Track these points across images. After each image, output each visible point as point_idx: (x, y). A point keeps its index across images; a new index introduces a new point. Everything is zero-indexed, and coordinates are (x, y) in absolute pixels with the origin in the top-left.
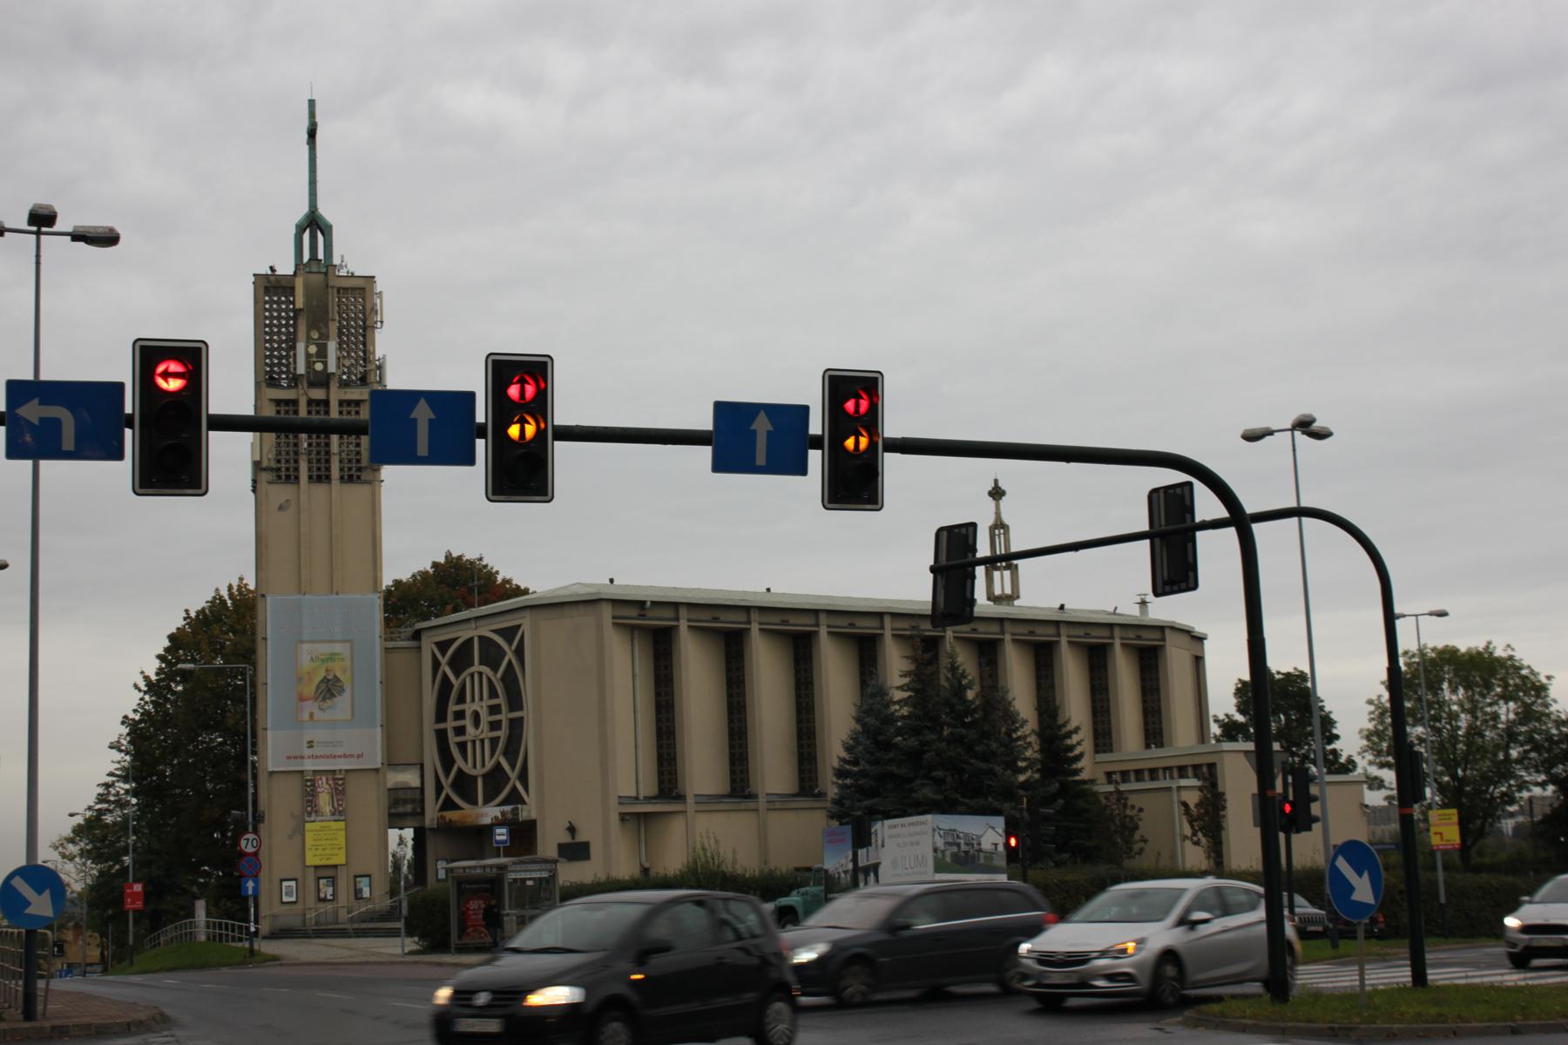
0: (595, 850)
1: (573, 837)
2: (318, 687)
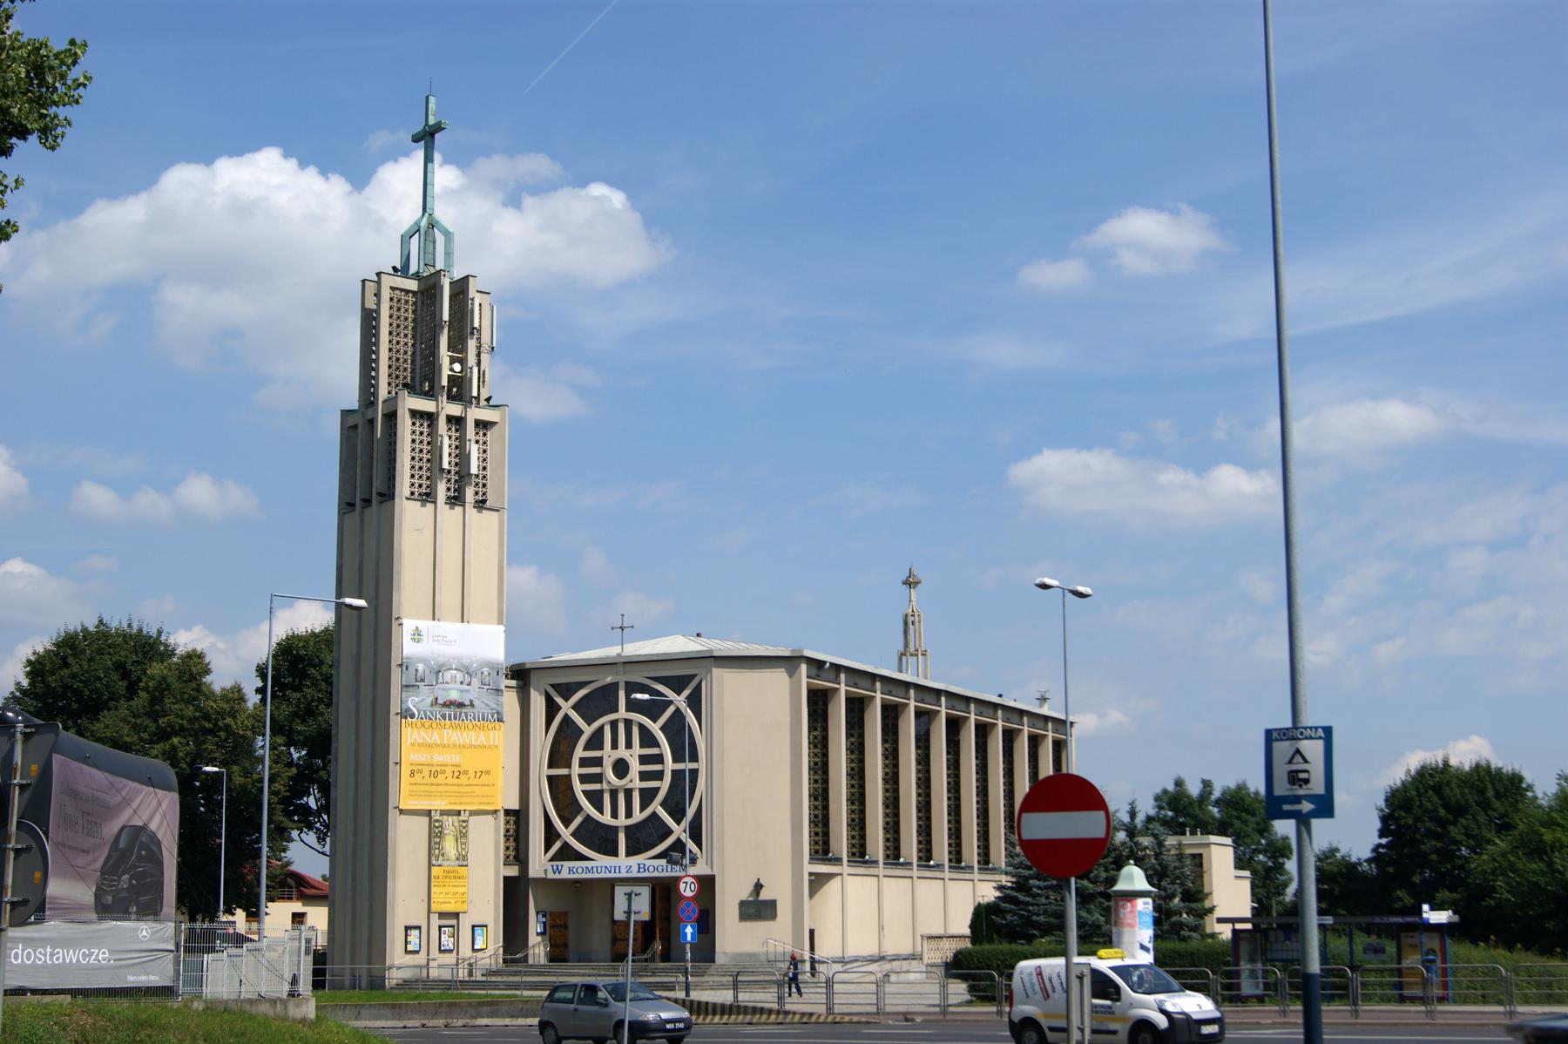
0: (784, 909)
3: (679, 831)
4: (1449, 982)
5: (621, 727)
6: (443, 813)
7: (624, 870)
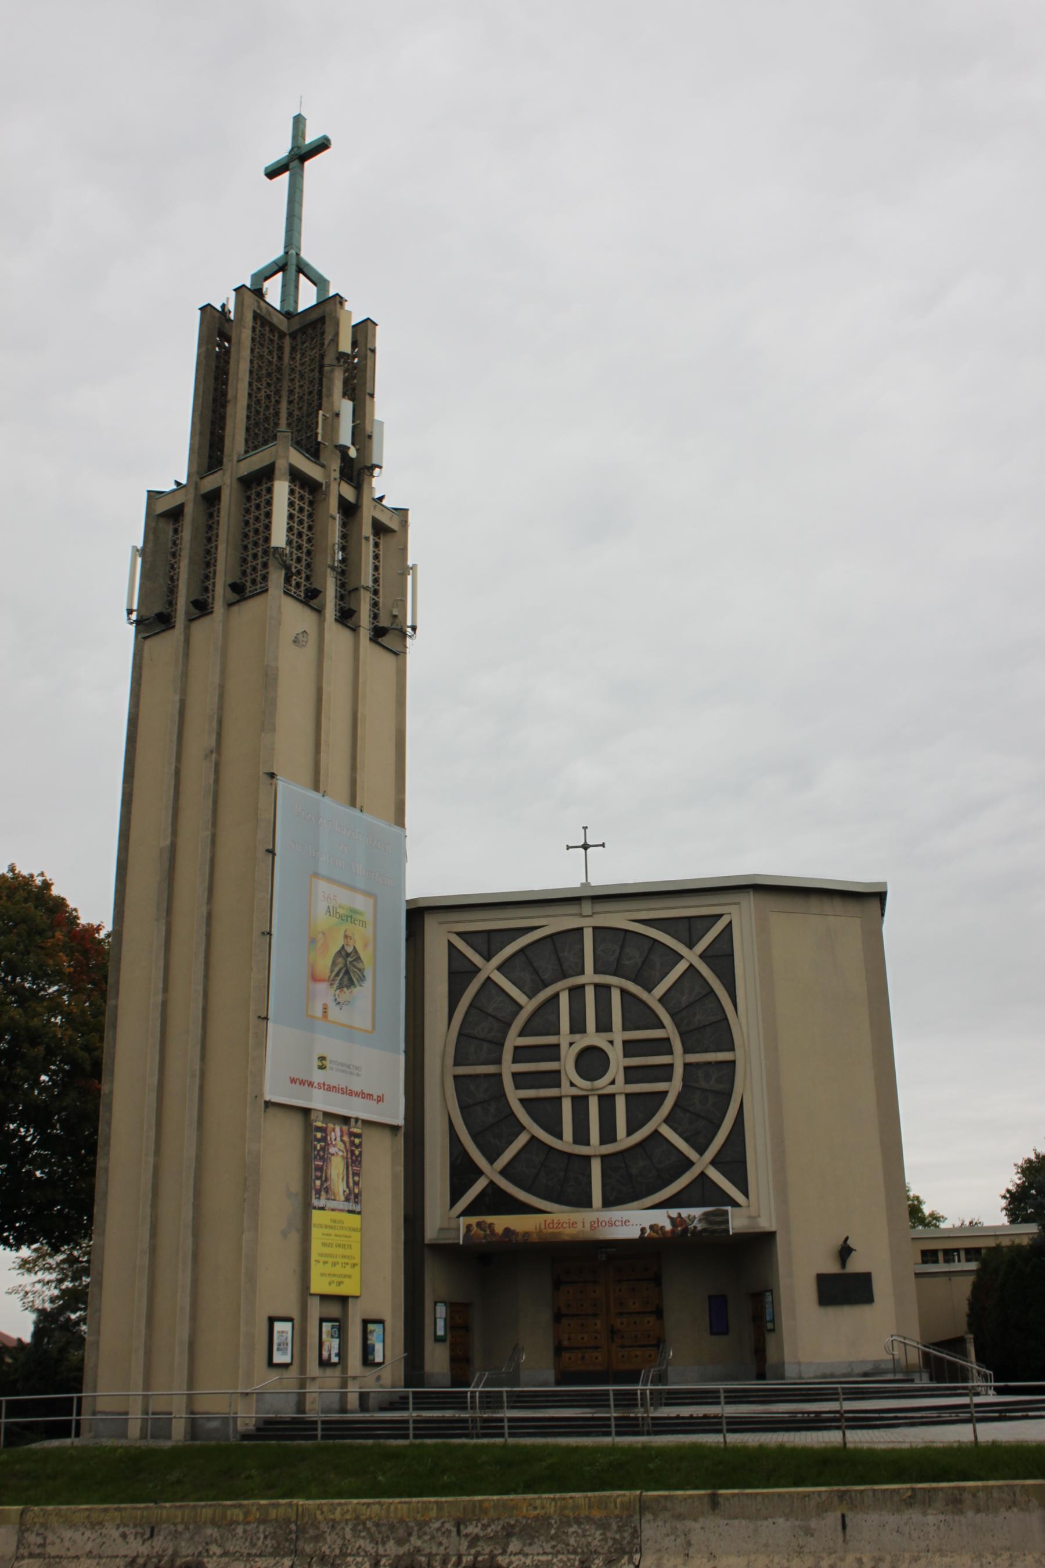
1: (843, 1265)
2: (334, 964)
5: (590, 994)
6: (328, 1116)
7: (580, 1226)
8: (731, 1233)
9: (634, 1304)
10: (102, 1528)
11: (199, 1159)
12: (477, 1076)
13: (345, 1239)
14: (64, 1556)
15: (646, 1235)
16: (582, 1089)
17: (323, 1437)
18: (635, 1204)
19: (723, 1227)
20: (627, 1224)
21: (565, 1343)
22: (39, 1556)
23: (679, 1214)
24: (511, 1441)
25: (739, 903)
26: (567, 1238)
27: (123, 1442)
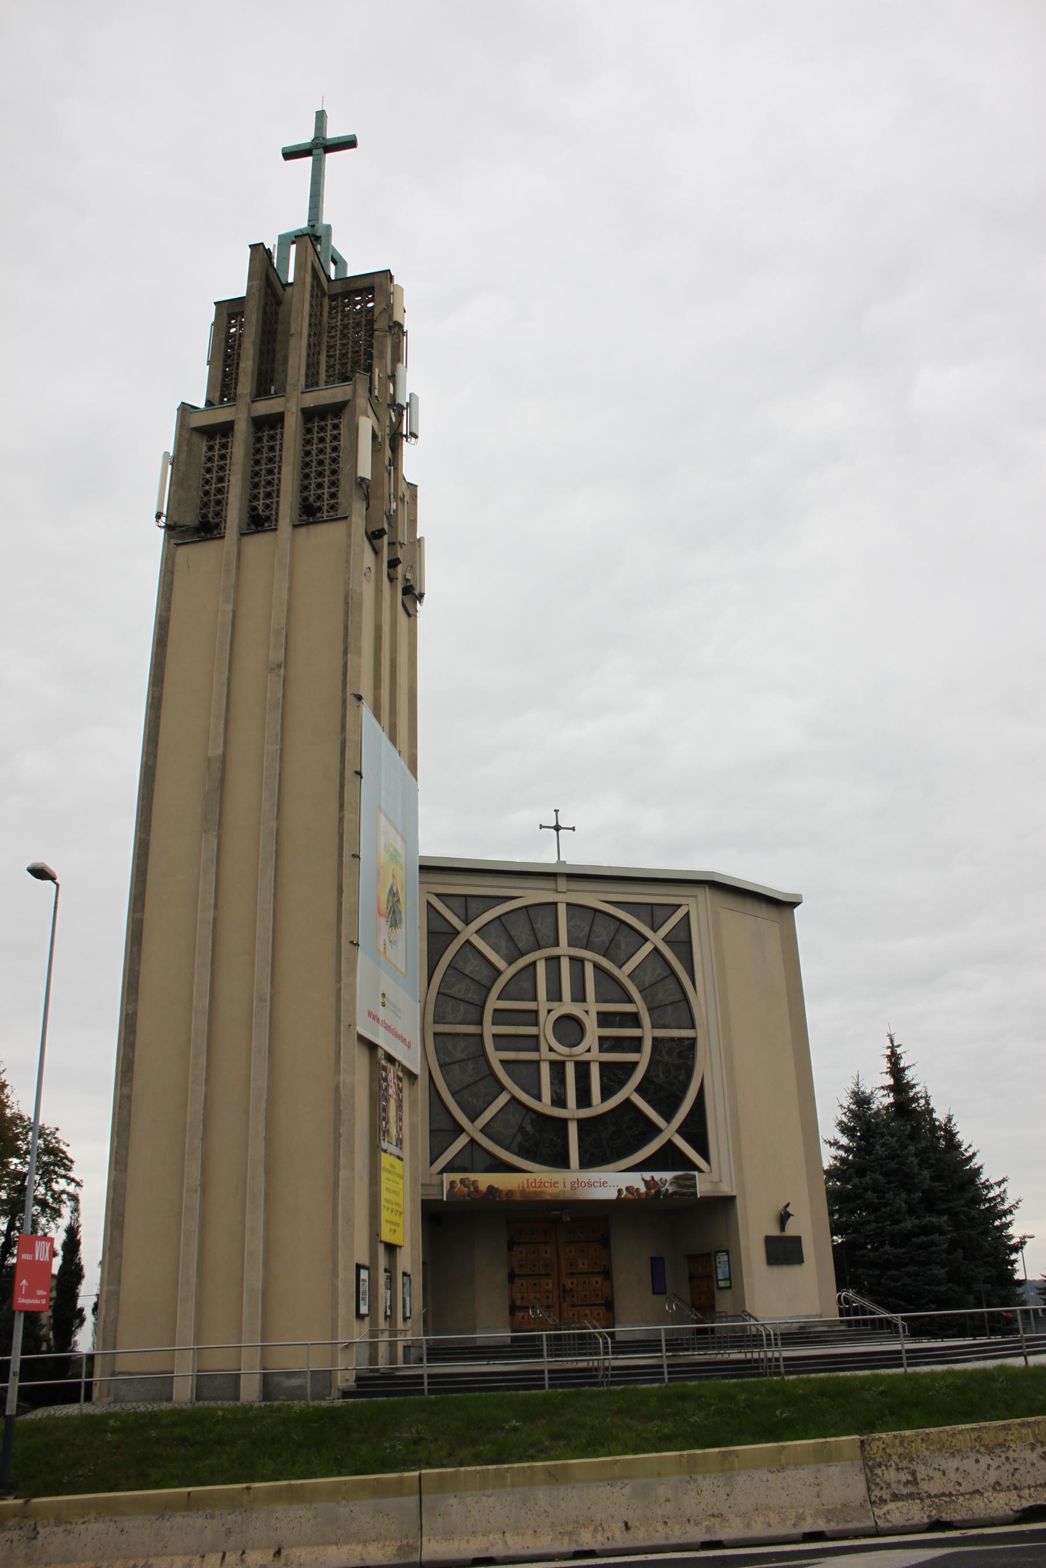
3: (670, 1131)
4: (259, 1340)
5: (565, 964)
7: (561, 1185)
8: (699, 1197)
9: (583, 1264)
10: (1007, 1451)
11: (270, 1090)
12: (457, 1035)
13: (393, 1184)
14: (954, 1493)
15: (623, 1196)
16: (560, 1054)
17: (551, 1386)
18: (611, 1166)
19: (691, 1190)
20: (605, 1185)
21: (518, 1303)
22: (911, 1496)
23: (652, 1177)
24: (910, 1370)
25: (695, 897)
26: (549, 1197)
27: (165, 1406)
